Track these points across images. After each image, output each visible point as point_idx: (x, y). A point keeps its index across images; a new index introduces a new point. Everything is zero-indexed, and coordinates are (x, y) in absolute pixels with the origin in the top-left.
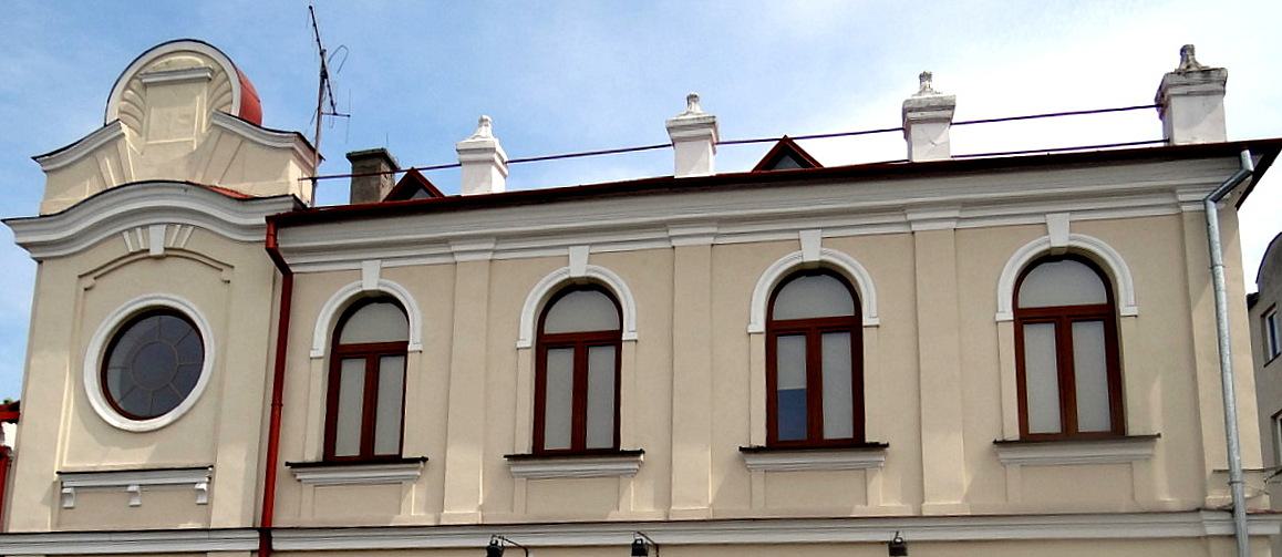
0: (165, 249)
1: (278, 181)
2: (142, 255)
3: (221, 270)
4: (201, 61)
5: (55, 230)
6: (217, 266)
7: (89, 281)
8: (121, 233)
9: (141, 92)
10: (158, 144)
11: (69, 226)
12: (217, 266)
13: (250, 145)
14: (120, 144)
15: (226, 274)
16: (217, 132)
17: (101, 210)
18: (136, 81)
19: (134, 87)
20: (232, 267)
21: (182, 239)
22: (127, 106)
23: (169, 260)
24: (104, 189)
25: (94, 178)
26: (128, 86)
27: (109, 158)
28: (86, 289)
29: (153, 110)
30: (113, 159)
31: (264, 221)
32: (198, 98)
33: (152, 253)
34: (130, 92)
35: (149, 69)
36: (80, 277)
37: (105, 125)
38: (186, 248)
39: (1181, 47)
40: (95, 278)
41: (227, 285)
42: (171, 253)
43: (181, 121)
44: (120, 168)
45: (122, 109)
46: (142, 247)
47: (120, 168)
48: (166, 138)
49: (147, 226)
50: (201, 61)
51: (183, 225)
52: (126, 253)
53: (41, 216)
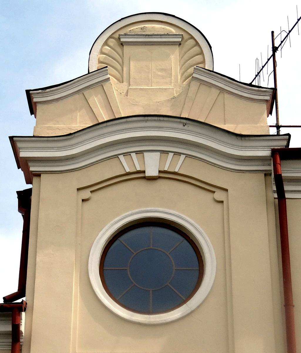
0: (160, 172)
1: (258, 125)
2: (140, 176)
3: (214, 192)
4: (173, 31)
5: (59, 149)
6: (208, 188)
7: (86, 194)
8: (117, 156)
9: (119, 49)
10: (141, 89)
11: (72, 146)
12: (208, 188)
13: (227, 96)
14: (106, 86)
15: (219, 195)
16: (195, 85)
17: (159, 128)
18: (111, 40)
19: (111, 44)
20: (226, 190)
21: (178, 165)
22: (105, 58)
23: (160, 182)
24: (97, 123)
25: (84, 111)
26: (106, 43)
27: (96, 96)
28: (83, 200)
29: (132, 63)
30: (99, 96)
31: (267, 153)
32: (172, 57)
33: (148, 174)
34: (107, 47)
35: (128, 30)
36: (78, 189)
37: (89, 73)
38: (180, 172)
39: (290, 134)
40: (91, 192)
41: (219, 206)
42: (165, 175)
43: (160, 73)
44: (108, 104)
45: (102, 60)
46: (138, 169)
47: (108, 104)
48: (148, 85)
49: (141, 152)
50: (173, 31)
51: (175, 153)
52: (124, 173)
53: (34, 137)
